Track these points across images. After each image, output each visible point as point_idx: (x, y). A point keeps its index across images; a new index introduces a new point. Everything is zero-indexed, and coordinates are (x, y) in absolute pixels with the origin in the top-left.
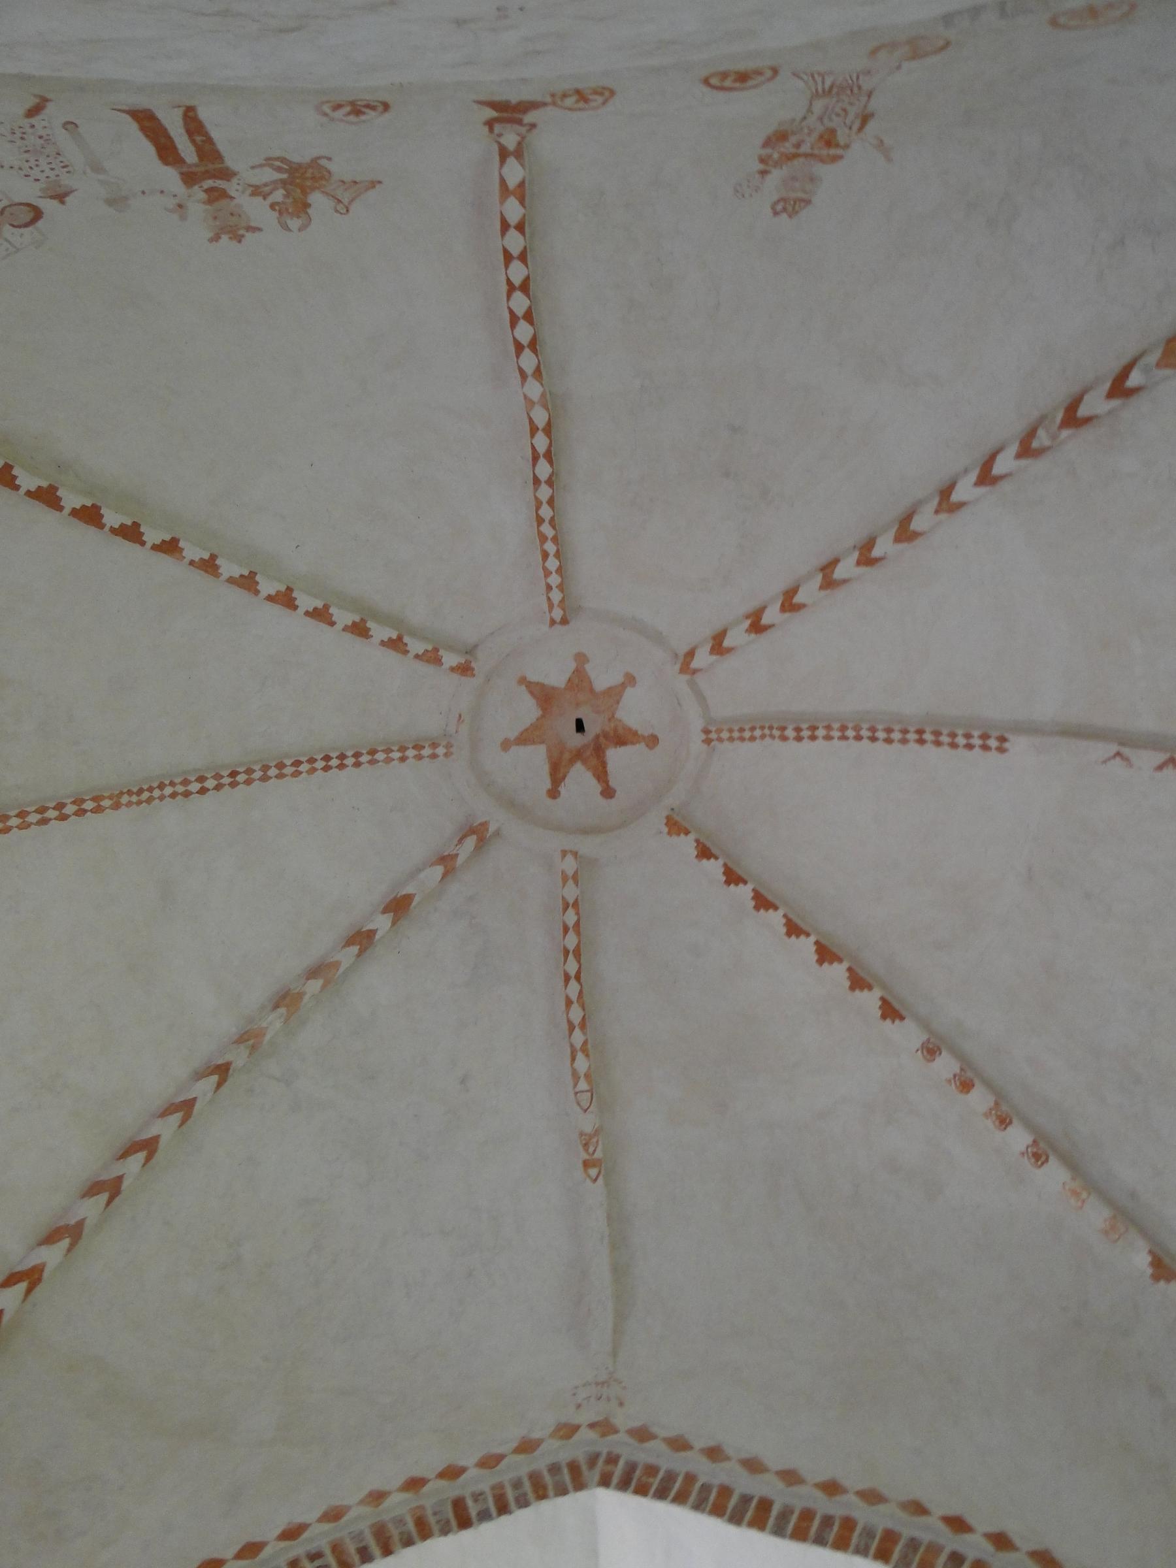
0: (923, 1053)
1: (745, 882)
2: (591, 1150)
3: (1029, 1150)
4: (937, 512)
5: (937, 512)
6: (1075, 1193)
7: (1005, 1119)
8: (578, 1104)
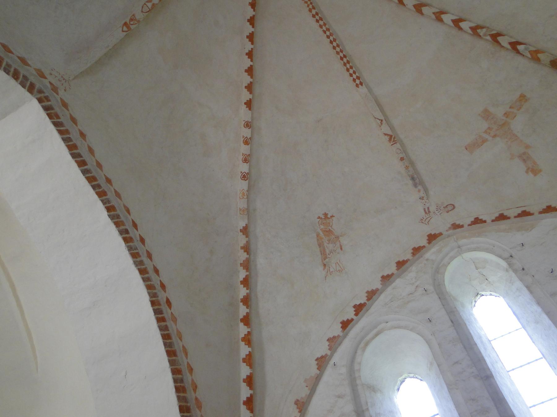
0: (245, 123)
1: (253, 27)
2: (132, 23)
3: (244, 173)
4: (434, 13)
5: (434, 13)
6: (243, 194)
7: (247, 160)
8: (142, 7)
